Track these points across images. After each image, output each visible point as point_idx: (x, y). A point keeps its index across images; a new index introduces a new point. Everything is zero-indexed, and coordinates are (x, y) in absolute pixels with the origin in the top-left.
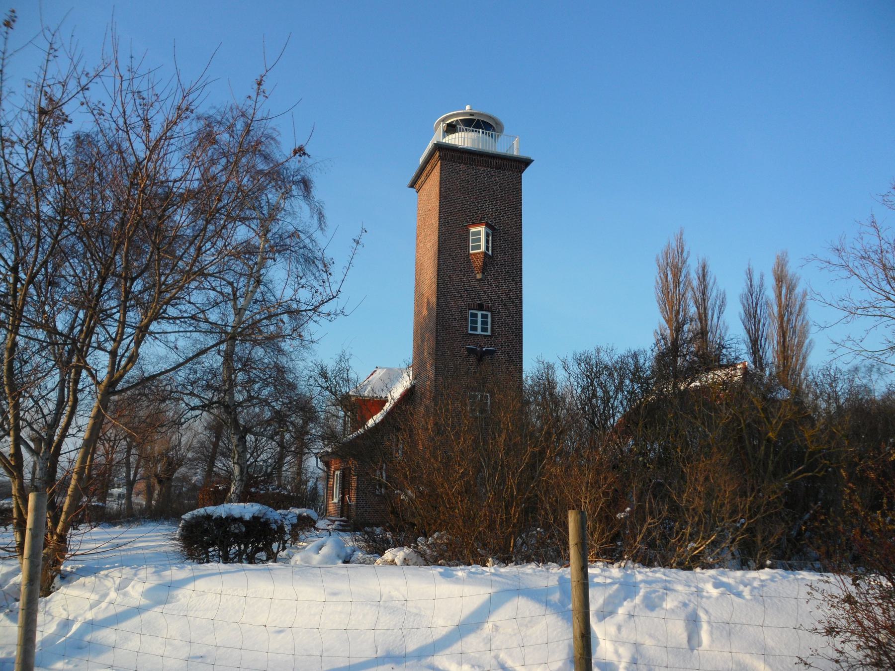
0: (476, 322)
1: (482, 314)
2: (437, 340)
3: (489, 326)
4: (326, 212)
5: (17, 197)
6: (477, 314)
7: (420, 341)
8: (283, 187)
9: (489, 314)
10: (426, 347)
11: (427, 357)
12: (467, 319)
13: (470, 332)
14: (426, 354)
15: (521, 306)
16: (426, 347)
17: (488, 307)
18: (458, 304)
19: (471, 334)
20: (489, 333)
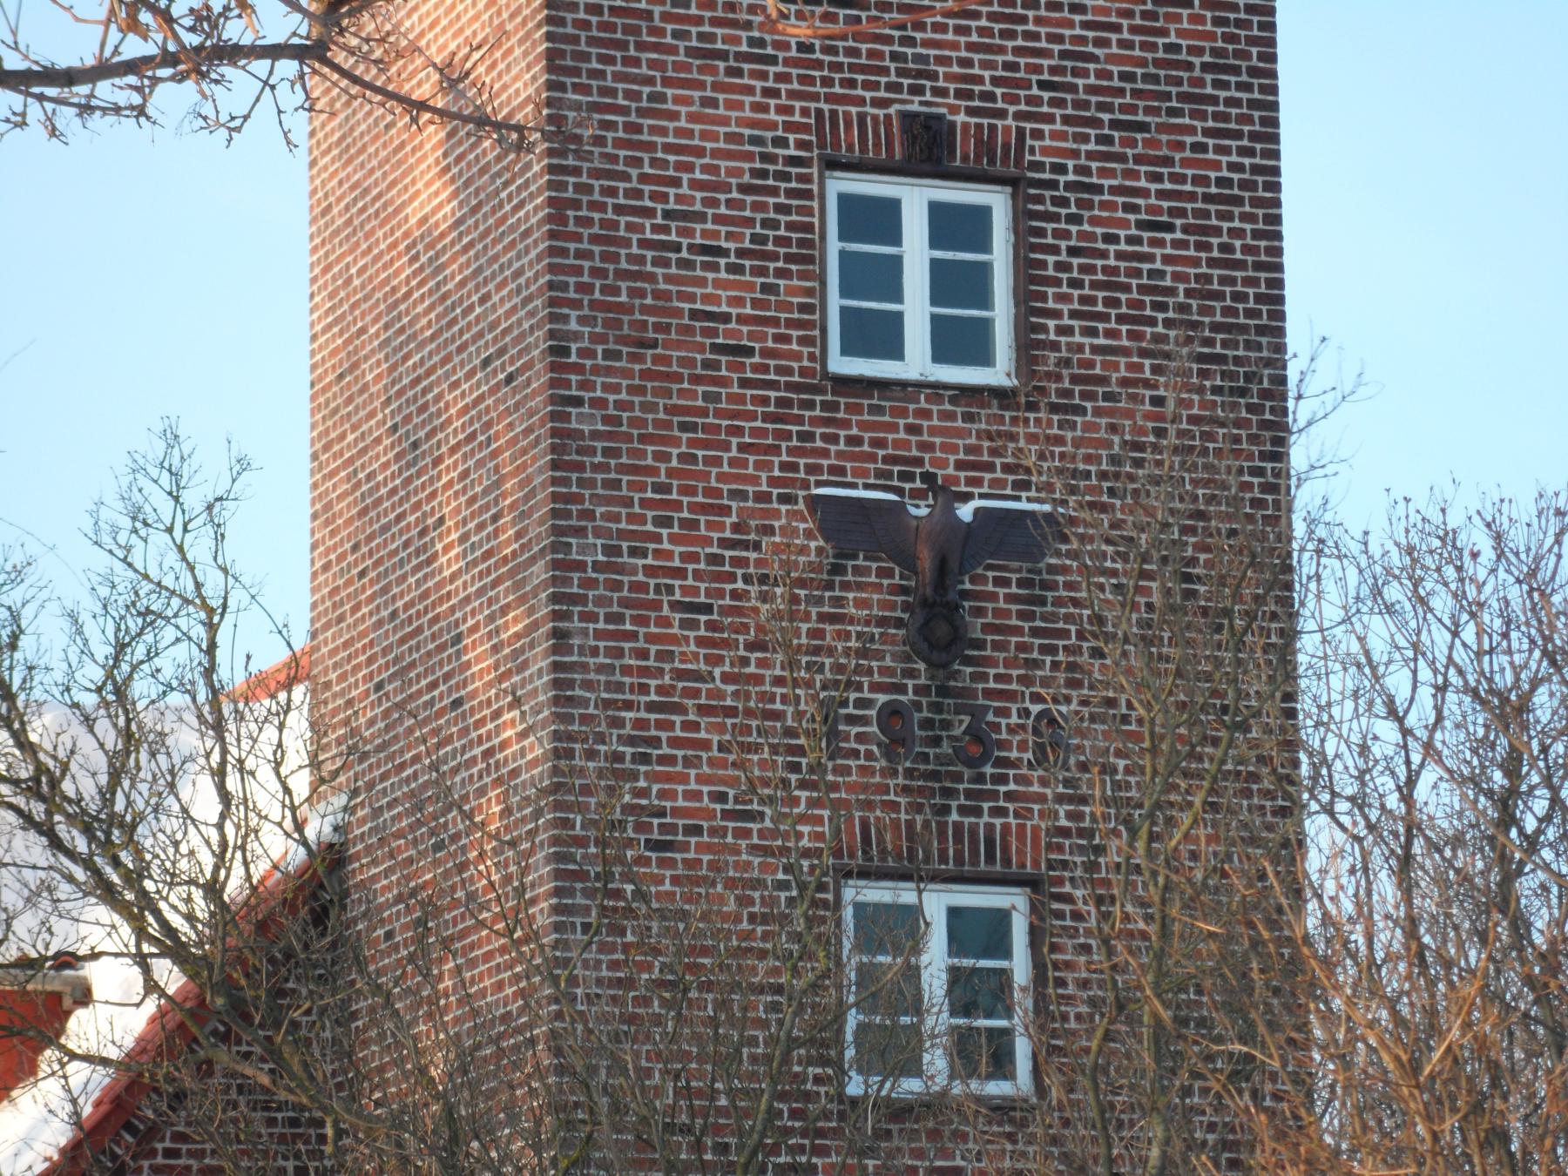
0: (888, 277)
1: (937, 211)
2: (562, 437)
3: (1002, 313)
4: (229, 531)
5: (1310, 814)
6: (892, 207)
7: (385, 452)
8: (746, 1153)
9: (997, 202)
10: (449, 506)
11: (466, 587)
12: (808, 256)
13: (841, 365)
14: (449, 561)
15: (1269, 135)
16: (449, 506)
17: (986, 146)
18: (736, 116)
19: (845, 384)
20: (999, 373)
